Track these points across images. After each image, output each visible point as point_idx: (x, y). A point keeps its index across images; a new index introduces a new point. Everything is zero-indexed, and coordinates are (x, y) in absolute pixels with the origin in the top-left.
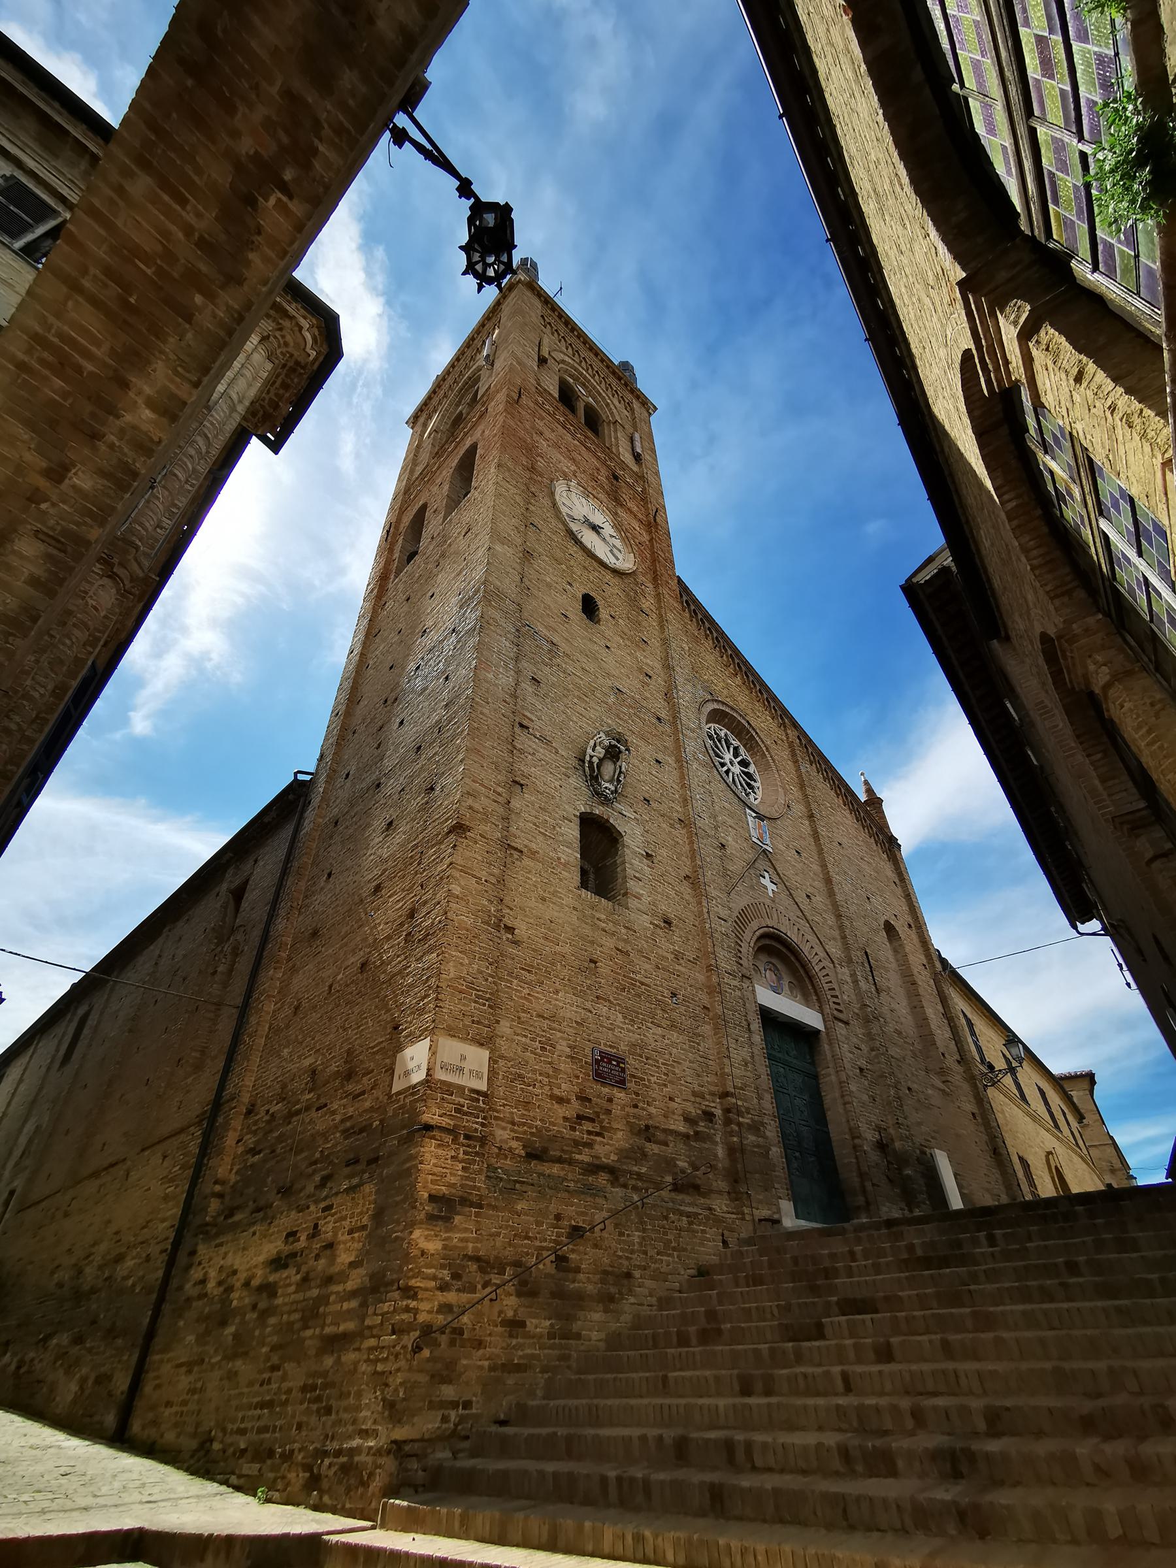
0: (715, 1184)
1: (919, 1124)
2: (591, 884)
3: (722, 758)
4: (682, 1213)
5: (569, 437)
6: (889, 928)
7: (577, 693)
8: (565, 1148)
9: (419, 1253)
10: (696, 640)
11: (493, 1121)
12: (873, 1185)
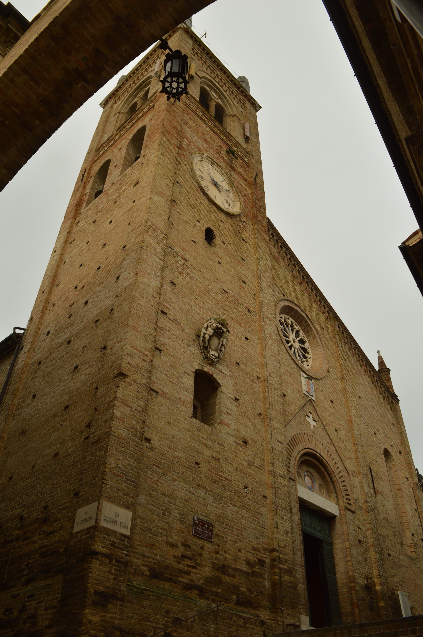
0: (262, 602)
1: (393, 576)
2: (199, 415)
3: (288, 337)
4: (240, 617)
5: (204, 126)
6: (387, 453)
7: (198, 292)
8: (174, 573)
9: (87, 622)
10: (277, 259)
11: (132, 554)
12: (360, 610)
